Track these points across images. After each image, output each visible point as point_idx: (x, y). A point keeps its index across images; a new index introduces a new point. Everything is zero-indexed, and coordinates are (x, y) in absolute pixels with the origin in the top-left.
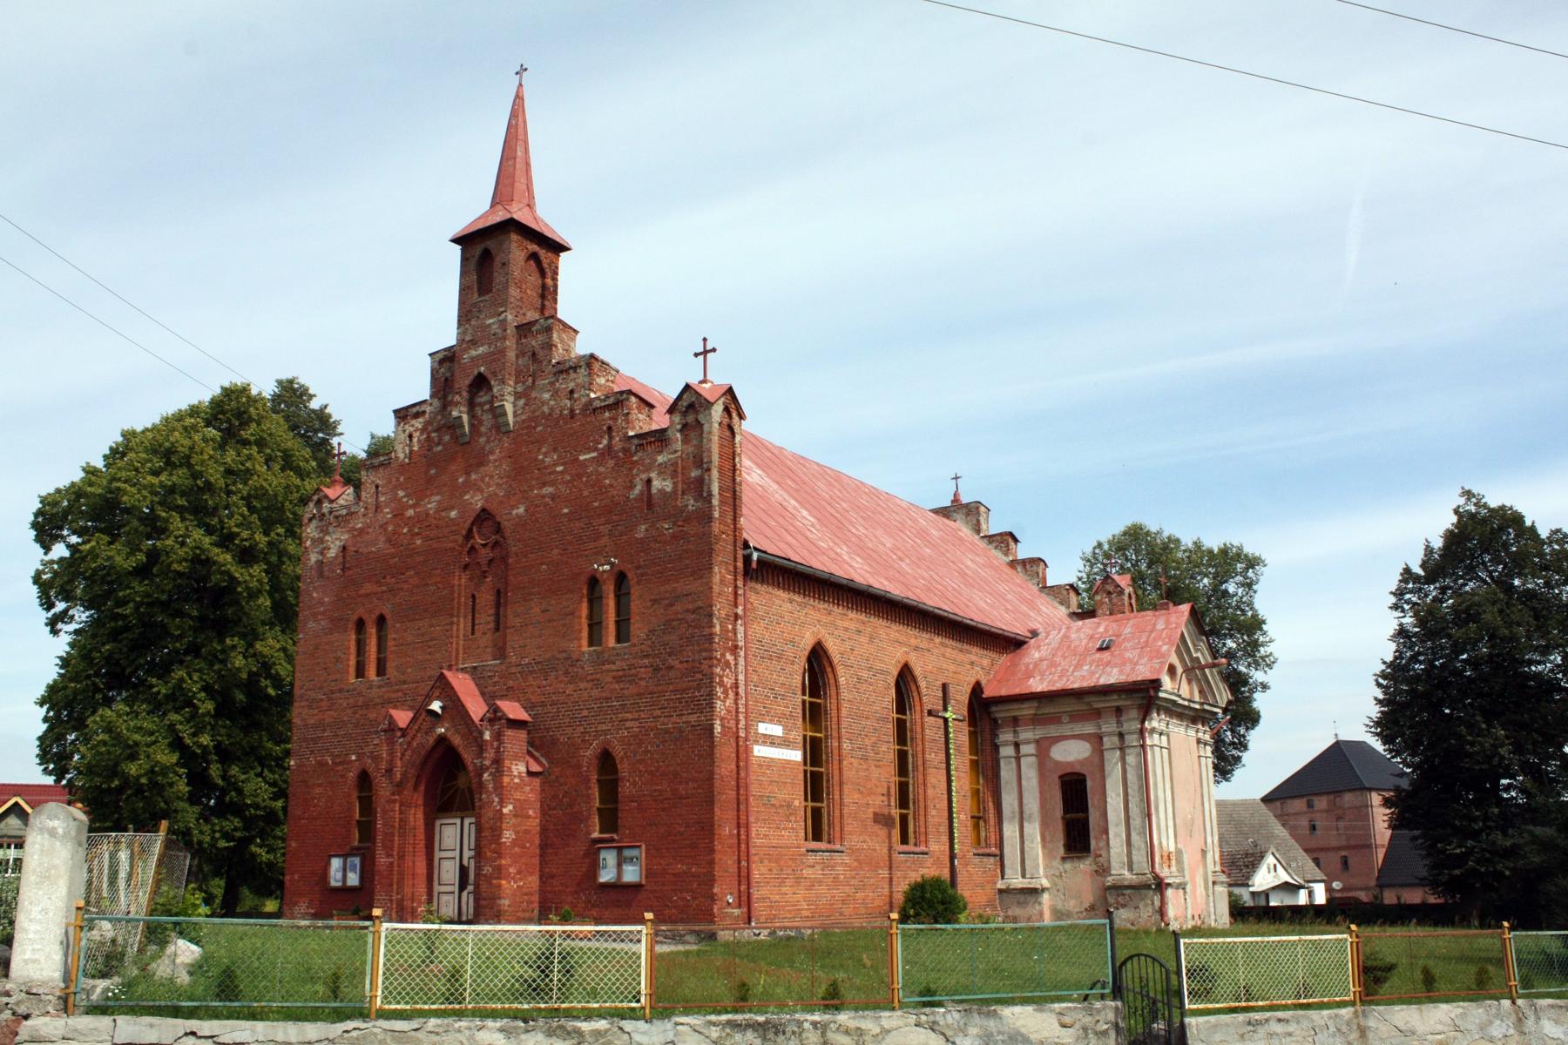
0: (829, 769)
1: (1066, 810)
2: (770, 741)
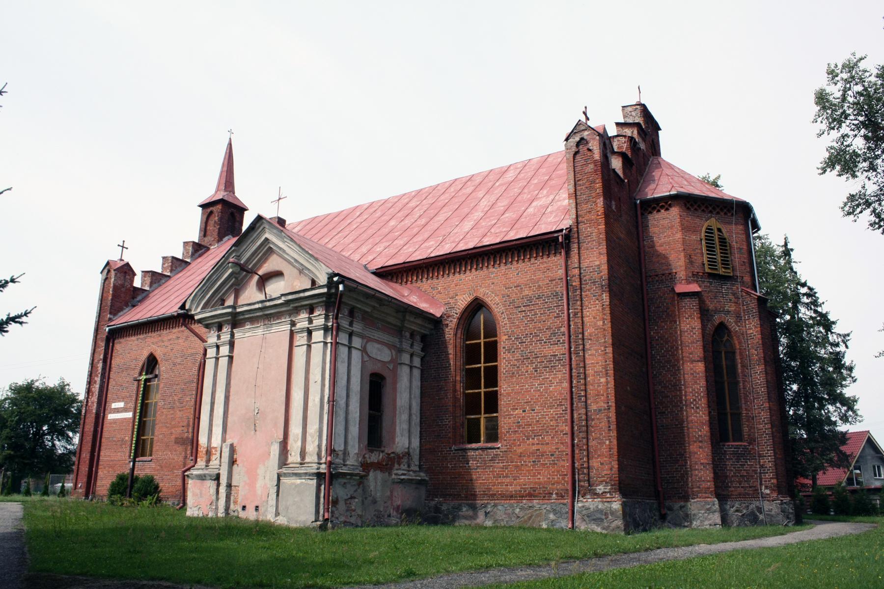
0: (149, 419)
1: (380, 417)
2: (117, 411)
